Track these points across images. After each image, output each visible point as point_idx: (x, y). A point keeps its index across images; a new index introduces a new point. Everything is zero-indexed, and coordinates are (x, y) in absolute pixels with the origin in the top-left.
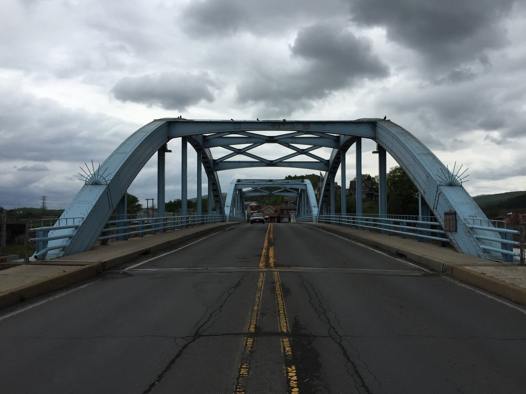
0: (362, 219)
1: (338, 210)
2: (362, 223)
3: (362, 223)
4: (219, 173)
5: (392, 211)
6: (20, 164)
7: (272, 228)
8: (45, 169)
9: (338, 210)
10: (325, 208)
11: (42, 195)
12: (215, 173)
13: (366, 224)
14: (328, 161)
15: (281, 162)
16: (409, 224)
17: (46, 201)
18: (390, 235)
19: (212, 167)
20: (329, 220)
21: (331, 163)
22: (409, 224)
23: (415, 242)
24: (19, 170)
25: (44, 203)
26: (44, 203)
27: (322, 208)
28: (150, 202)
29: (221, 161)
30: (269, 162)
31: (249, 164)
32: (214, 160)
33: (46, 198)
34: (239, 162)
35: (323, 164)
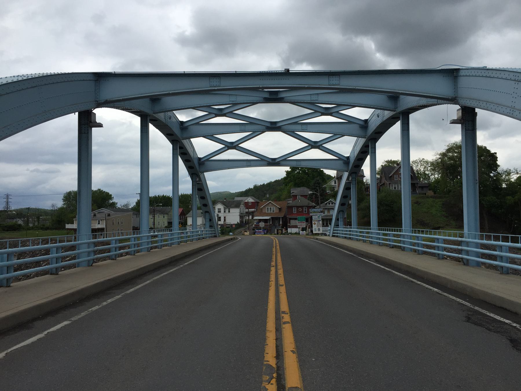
0: (357, 232)
1: (365, 222)
2: (357, 235)
3: (357, 235)
4: (206, 174)
5: (420, 223)
6: (32, 167)
7: (278, 245)
8: (58, 171)
9: (365, 222)
10: (342, 219)
11: (6, 193)
12: (201, 176)
13: (361, 236)
14: (348, 158)
15: (285, 160)
16: (394, 236)
17: (10, 200)
18: (439, 259)
19: (197, 167)
20: (460, 252)
21: (352, 161)
22: (394, 236)
23: (495, 274)
24: (32, 171)
25: (7, 203)
26: (7, 203)
27: (338, 220)
28: (284, 231)
29: (208, 160)
30: (270, 161)
31: (245, 163)
32: (200, 159)
33: (10, 197)
34: (229, 160)
35: (341, 162)
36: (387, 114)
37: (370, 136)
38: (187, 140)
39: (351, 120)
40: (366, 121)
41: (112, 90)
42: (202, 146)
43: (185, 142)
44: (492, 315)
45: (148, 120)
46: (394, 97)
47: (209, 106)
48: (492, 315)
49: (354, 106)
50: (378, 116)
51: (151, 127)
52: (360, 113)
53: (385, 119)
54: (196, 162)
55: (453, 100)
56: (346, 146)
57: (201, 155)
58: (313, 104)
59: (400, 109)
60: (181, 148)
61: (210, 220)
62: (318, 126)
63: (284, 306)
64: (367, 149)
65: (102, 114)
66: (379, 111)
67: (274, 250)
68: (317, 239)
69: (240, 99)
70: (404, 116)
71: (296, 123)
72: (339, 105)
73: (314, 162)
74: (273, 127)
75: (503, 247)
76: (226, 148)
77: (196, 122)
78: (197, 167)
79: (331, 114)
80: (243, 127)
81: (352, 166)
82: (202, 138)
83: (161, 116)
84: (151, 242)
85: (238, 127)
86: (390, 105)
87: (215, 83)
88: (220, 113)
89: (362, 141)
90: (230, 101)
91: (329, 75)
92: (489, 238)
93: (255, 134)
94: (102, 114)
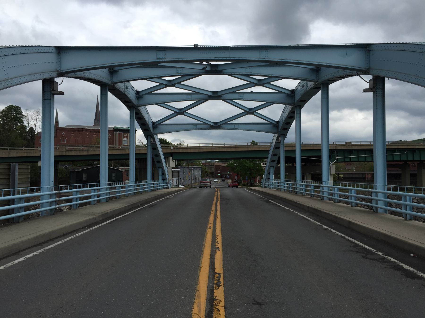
14: (278, 122)
29: (160, 124)
31: (191, 126)
32: (154, 123)
36: (310, 84)
37: (295, 102)
38: (143, 107)
39: (280, 91)
40: (293, 91)
41: (70, 62)
42: (155, 112)
43: (142, 109)
44: (412, 269)
45: (107, 90)
46: (317, 69)
47: (159, 78)
48: (412, 269)
49: (283, 78)
50: (303, 87)
51: (110, 95)
52: (290, 84)
53: (309, 88)
54: (150, 125)
55: (366, 72)
56: (276, 112)
57: (155, 120)
58: (247, 75)
59: (320, 81)
60: (137, 114)
61: (163, 174)
62: (180, 95)
63: (219, 268)
64: (293, 115)
65: (64, 84)
66: (304, 82)
67: (215, 198)
68: (252, 189)
69: (186, 72)
70: (323, 86)
71: (233, 93)
72: (270, 77)
73: (262, 95)
74: (216, 96)
75: (409, 198)
76: (176, 114)
77: (150, 91)
78: (150, 130)
79: (263, 85)
80: (189, 96)
81: (280, 128)
82: (155, 106)
83: (120, 86)
84: (110, 193)
85: (185, 97)
86: (313, 77)
87: (161, 56)
88: (171, 84)
89: (289, 108)
90: (177, 73)
91: (261, 50)
92: (395, 189)
93: (199, 102)
94: (64, 84)
